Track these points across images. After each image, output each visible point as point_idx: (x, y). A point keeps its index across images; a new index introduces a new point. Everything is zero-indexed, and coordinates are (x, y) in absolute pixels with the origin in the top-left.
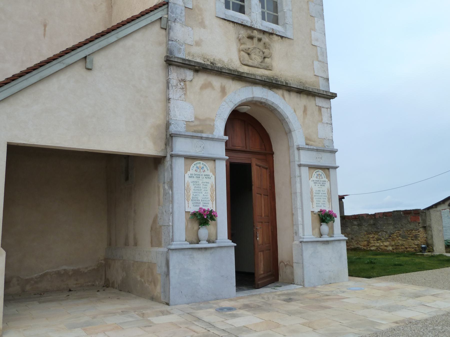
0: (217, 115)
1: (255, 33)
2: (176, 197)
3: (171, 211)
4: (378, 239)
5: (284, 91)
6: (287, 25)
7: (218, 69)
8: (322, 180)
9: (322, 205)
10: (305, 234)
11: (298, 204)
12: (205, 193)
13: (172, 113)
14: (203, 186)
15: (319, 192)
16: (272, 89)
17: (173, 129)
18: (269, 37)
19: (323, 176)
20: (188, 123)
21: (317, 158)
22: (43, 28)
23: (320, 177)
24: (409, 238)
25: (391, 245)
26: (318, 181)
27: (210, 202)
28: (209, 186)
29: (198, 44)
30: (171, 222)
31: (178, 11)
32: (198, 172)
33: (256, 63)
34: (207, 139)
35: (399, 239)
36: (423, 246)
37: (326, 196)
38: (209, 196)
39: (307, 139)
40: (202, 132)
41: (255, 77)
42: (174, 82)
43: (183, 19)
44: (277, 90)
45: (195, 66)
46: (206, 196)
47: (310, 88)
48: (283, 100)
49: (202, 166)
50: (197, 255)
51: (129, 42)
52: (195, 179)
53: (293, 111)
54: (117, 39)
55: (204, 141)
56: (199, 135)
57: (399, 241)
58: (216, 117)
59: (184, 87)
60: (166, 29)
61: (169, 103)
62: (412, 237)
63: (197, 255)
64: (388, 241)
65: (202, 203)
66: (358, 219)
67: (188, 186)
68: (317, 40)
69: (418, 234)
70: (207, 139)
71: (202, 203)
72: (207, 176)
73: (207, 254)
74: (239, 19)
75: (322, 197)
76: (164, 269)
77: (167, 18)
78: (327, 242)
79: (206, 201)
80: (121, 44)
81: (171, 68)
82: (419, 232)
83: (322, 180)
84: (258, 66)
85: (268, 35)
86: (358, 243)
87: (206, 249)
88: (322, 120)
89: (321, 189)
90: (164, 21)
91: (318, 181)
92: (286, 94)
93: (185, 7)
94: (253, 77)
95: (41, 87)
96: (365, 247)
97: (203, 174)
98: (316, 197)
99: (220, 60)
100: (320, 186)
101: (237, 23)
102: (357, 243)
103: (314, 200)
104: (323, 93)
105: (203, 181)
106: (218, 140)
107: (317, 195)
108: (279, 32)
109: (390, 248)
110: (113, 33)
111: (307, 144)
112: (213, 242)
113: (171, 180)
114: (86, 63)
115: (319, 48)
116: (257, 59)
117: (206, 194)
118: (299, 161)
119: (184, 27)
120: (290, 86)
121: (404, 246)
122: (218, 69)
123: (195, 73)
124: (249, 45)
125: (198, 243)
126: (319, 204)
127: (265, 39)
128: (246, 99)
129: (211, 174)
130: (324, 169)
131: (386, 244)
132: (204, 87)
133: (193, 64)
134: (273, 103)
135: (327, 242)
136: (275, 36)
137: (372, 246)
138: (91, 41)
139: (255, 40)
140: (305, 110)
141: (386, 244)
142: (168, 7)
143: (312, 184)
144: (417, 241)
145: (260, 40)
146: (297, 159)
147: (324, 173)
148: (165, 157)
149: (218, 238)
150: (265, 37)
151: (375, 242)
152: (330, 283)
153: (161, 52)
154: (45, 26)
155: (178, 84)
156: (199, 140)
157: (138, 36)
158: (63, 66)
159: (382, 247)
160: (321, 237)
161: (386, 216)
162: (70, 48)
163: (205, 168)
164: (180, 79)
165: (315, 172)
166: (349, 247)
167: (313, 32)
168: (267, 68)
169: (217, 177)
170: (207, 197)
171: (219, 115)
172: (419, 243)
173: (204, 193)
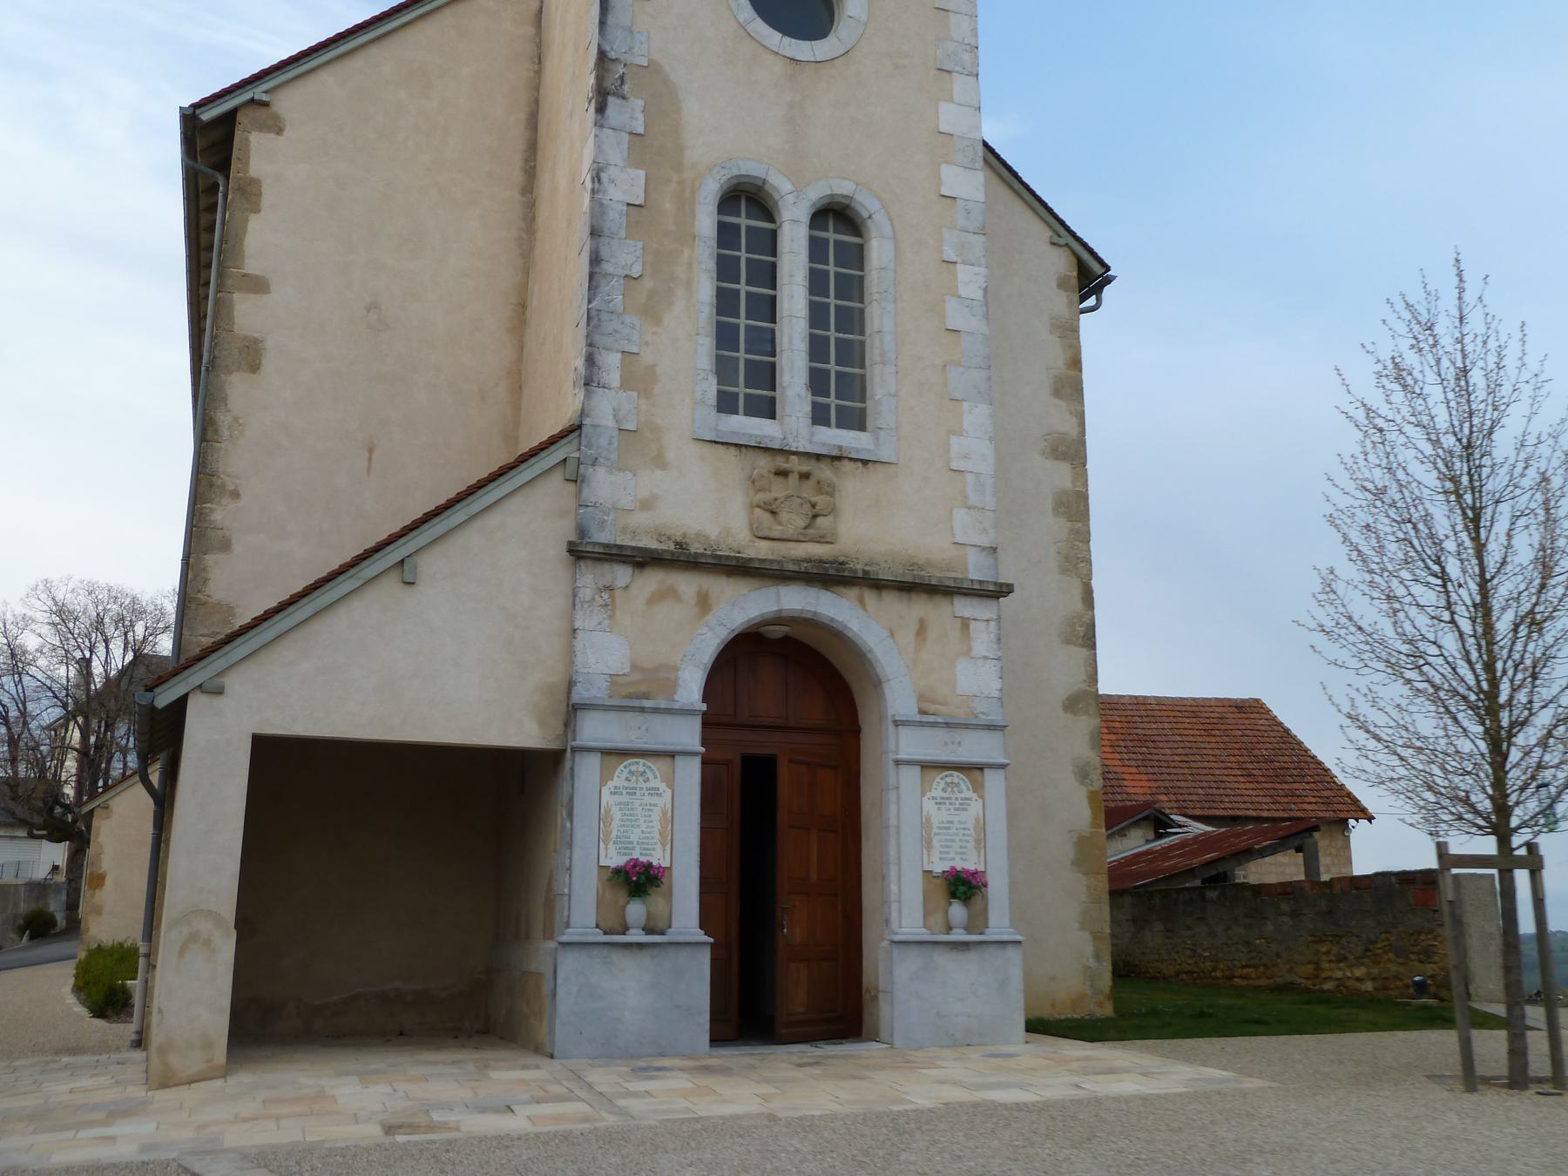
0: (685, 656)
1: (795, 464)
2: (579, 836)
3: (568, 865)
4: (1341, 959)
5: (864, 589)
6: (881, 432)
7: (688, 558)
8: (959, 796)
9: (958, 857)
10: (904, 923)
11: (892, 853)
12: (648, 827)
13: (579, 660)
14: (644, 813)
15: (948, 825)
16: (831, 586)
17: (580, 694)
18: (832, 465)
19: (963, 786)
20: (614, 678)
21: (946, 743)
22: (367, 456)
23: (955, 789)
24: (1413, 957)
25: (1372, 976)
26: (948, 799)
27: (659, 847)
28: (656, 814)
29: (647, 505)
30: (568, 886)
31: (604, 441)
32: (633, 781)
33: (790, 531)
34: (656, 710)
35: (1389, 960)
36: (1417, 979)
37: (970, 835)
38: (656, 835)
39: (921, 698)
40: (646, 696)
41: (783, 565)
42: (586, 593)
43: (614, 457)
44: (845, 587)
45: (634, 556)
46: (649, 833)
47: (935, 576)
48: (861, 611)
49: (641, 769)
50: (621, 960)
51: (493, 519)
52: (625, 798)
53: (886, 634)
54: (467, 517)
55: (648, 716)
56: (636, 703)
57: (1389, 965)
58: (682, 660)
59: (609, 601)
60: (576, 481)
61: (575, 638)
62: (1419, 954)
63: (618, 958)
64: (1362, 964)
65: (638, 848)
66: (1291, 896)
67: (608, 811)
68: (966, 457)
69: (1435, 943)
70: (656, 710)
71: (638, 848)
72: (654, 791)
73: (645, 959)
74: (751, 435)
75: (957, 838)
76: (552, 985)
77: (579, 458)
78: (965, 945)
79: (648, 844)
80: (477, 524)
81: (582, 564)
82: (1435, 938)
83: (959, 796)
84: (795, 537)
85: (829, 460)
86: (1292, 968)
87: (641, 946)
88: (970, 650)
89: (956, 819)
90: (571, 466)
91: (948, 799)
92: (870, 596)
93: (620, 430)
94: (775, 567)
95: (316, 626)
96: (1310, 982)
97: (645, 786)
98: (939, 837)
99: (698, 535)
100: (952, 811)
101: (746, 446)
102: (1291, 970)
103: (935, 843)
104: (970, 587)
105: (643, 802)
106: (687, 712)
107: (944, 831)
108: (857, 451)
109: (1368, 986)
110: (458, 506)
111: (922, 712)
112: (663, 933)
113: (571, 799)
114: (403, 572)
115: (970, 477)
116: (793, 520)
117: (648, 830)
118: (896, 752)
119: (616, 472)
120: (875, 577)
121: (1401, 980)
122: (688, 558)
123: (636, 570)
124: (778, 490)
125: (624, 934)
126: (947, 853)
127: (824, 472)
128: (762, 615)
129: (663, 787)
130: (970, 769)
131: (1359, 972)
132: (656, 599)
133: (629, 553)
134: (832, 620)
135: (965, 945)
136: (846, 462)
137: (1325, 979)
138: (412, 530)
139: (793, 479)
140: (922, 630)
141: (1359, 972)
142: (580, 435)
143: (929, 806)
144: (1432, 965)
145: (805, 476)
146: (892, 746)
147: (966, 780)
148: (565, 750)
149: (674, 924)
150: (823, 466)
151: (1333, 965)
152: (969, 1045)
153: (565, 531)
154: (371, 450)
155: (597, 597)
156: (637, 714)
157: (513, 504)
158: (358, 584)
159: (1350, 983)
160: (948, 934)
161: (1357, 888)
162: (371, 548)
163: (649, 774)
164: (600, 586)
165: (941, 776)
166: (1272, 981)
167: (954, 440)
168: (820, 540)
169: (675, 792)
170: (651, 835)
171: (690, 657)
172: (1434, 970)
173: (643, 826)
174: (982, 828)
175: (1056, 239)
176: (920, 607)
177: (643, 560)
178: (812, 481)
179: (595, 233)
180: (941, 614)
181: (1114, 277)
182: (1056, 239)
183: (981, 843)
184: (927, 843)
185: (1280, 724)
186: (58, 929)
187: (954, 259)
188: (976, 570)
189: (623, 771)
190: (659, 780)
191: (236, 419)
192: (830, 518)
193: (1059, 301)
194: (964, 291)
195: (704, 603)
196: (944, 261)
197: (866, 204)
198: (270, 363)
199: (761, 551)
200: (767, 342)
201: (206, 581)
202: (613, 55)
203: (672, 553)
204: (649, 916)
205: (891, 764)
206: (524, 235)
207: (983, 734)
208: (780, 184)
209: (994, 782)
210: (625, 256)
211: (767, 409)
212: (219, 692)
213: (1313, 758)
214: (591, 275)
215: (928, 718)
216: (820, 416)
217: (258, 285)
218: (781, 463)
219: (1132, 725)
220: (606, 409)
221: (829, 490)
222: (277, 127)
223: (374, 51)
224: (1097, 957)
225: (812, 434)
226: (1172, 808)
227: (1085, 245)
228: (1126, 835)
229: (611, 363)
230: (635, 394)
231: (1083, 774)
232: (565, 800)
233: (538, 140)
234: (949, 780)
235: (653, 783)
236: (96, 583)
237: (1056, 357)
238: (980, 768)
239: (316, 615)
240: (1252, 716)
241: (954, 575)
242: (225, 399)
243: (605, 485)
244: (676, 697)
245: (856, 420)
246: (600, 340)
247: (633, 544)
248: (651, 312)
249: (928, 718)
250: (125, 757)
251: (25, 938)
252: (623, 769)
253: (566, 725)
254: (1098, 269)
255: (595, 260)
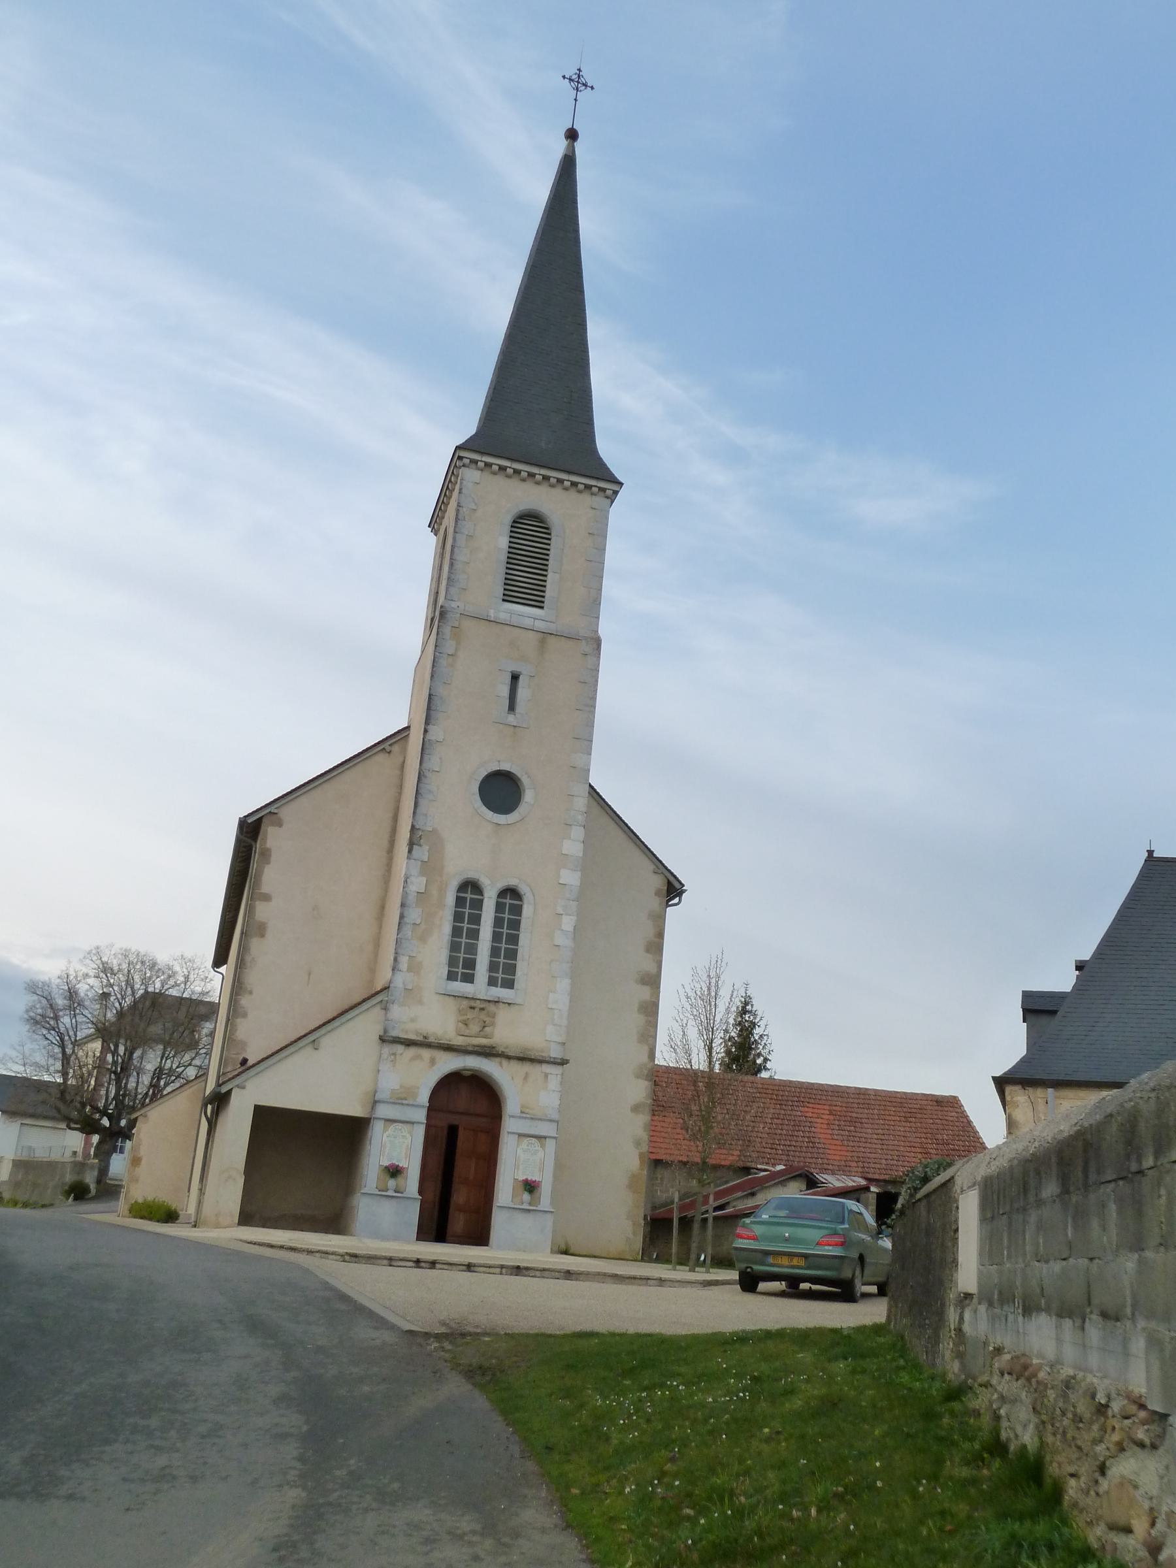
1: (478, 1004)
17: (378, 1096)
29: (413, 1020)
39: (522, 1106)
42: (385, 1056)
47: (532, 1055)
48: (500, 1068)
51: (351, 1024)
56: (400, 1101)
73: (394, 1201)
78: (529, 1211)
87: (393, 1197)
92: (505, 1062)
101: (458, 997)
103: (521, 1167)
111: (522, 1112)
112: (402, 1193)
116: (474, 1028)
124: (470, 1015)
127: (492, 1007)
129: (408, 1135)
132: (413, 1059)
153: (377, 1030)
154: (310, 974)
164: (391, 1052)
174: (543, 1163)
175: (656, 870)
176: (527, 1067)
177: (409, 1043)
178: (485, 1012)
179: (403, 905)
180: (536, 1071)
181: (686, 890)
182: (656, 870)
183: (542, 1170)
184: (516, 1167)
185: (967, 1117)
186: (90, 1195)
187: (562, 912)
188: (555, 1053)
189: (392, 1128)
190: (407, 1132)
191: (253, 958)
192: (491, 1028)
193: (655, 903)
194: (565, 927)
195: (433, 1062)
196: (557, 914)
197: (523, 889)
198: (269, 934)
199: (459, 1041)
200: (472, 949)
201: (236, 1030)
202: (417, 827)
203: (421, 1041)
204: (397, 1185)
205: (506, 1133)
206: (387, 874)
207: (548, 1123)
208: (485, 882)
209: (551, 1145)
210: (414, 915)
211: (469, 978)
212: (243, 1088)
213: (981, 1144)
214: (399, 923)
215: (524, 1114)
216: (492, 982)
217: (267, 898)
218: (473, 1004)
219: (850, 1109)
220: (399, 981)
221: (493, 1016)
222: (280, 824)
223: (326, 786)
224: (634, 1234)
225: (487, 991)
226: (857, 1172)
227: (672, 874)
228: (786, 1186)
229: (404, 962)
230: (413, 974)
231: (638, 1143)
232: (369, 1137)
233: (397, 828)
234: (530, 1142)
235: (404, 1134)
236: (130, 950)
237: (649, 931)
238: (545, 1138)
239: (279, 1061)
240: (946, 1109)
241: (543, 1054)
242: (249, 949)
243: (396, 1012)
244: (417, 1100)
245: (509, 984)
246: (400, 951)
247: (405, 1037)
248: (423, 939)
249: (524, 1114)
250: (74, 1047)
251: (71, 1199)
252: (393, 1127)
253: (372, 1109)
254: (677, 885)
255: (402, 917)
